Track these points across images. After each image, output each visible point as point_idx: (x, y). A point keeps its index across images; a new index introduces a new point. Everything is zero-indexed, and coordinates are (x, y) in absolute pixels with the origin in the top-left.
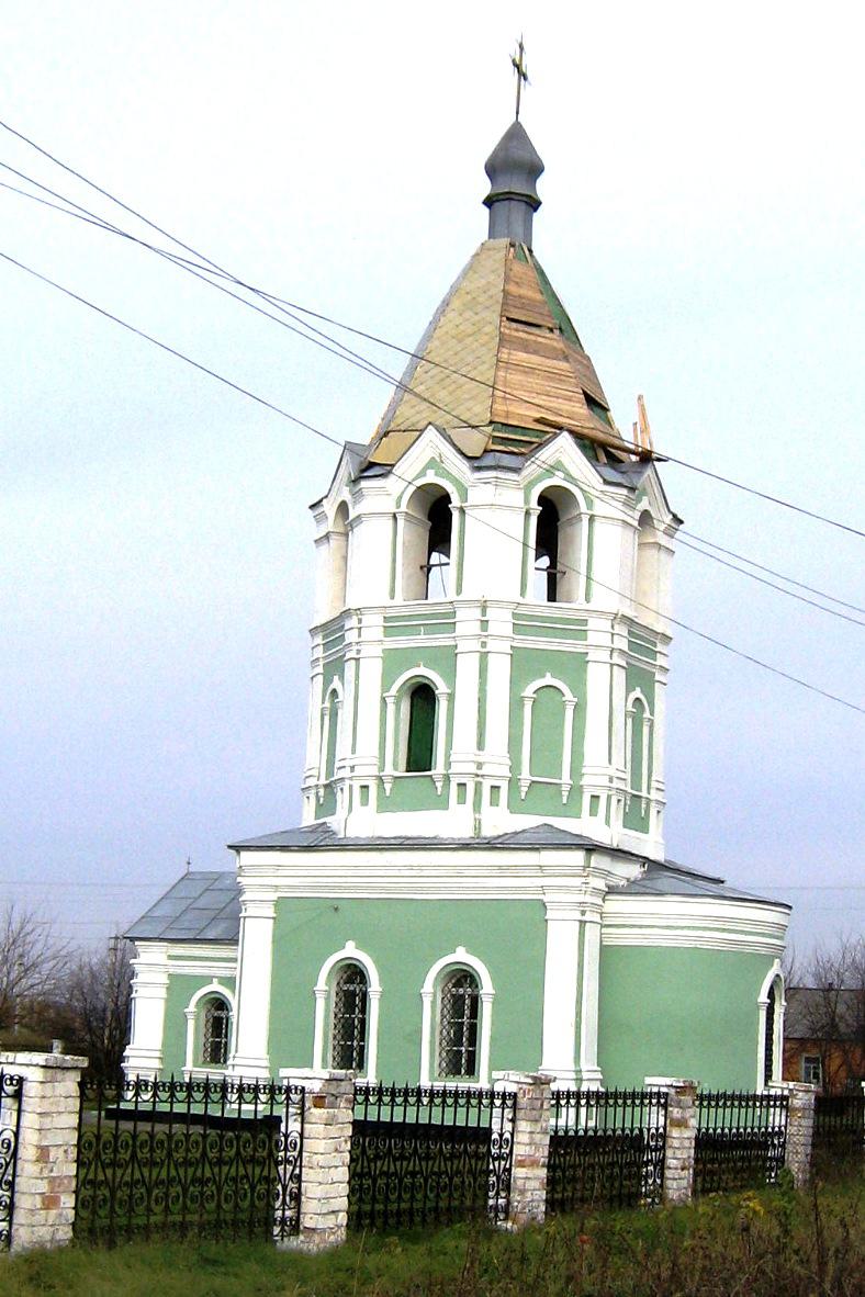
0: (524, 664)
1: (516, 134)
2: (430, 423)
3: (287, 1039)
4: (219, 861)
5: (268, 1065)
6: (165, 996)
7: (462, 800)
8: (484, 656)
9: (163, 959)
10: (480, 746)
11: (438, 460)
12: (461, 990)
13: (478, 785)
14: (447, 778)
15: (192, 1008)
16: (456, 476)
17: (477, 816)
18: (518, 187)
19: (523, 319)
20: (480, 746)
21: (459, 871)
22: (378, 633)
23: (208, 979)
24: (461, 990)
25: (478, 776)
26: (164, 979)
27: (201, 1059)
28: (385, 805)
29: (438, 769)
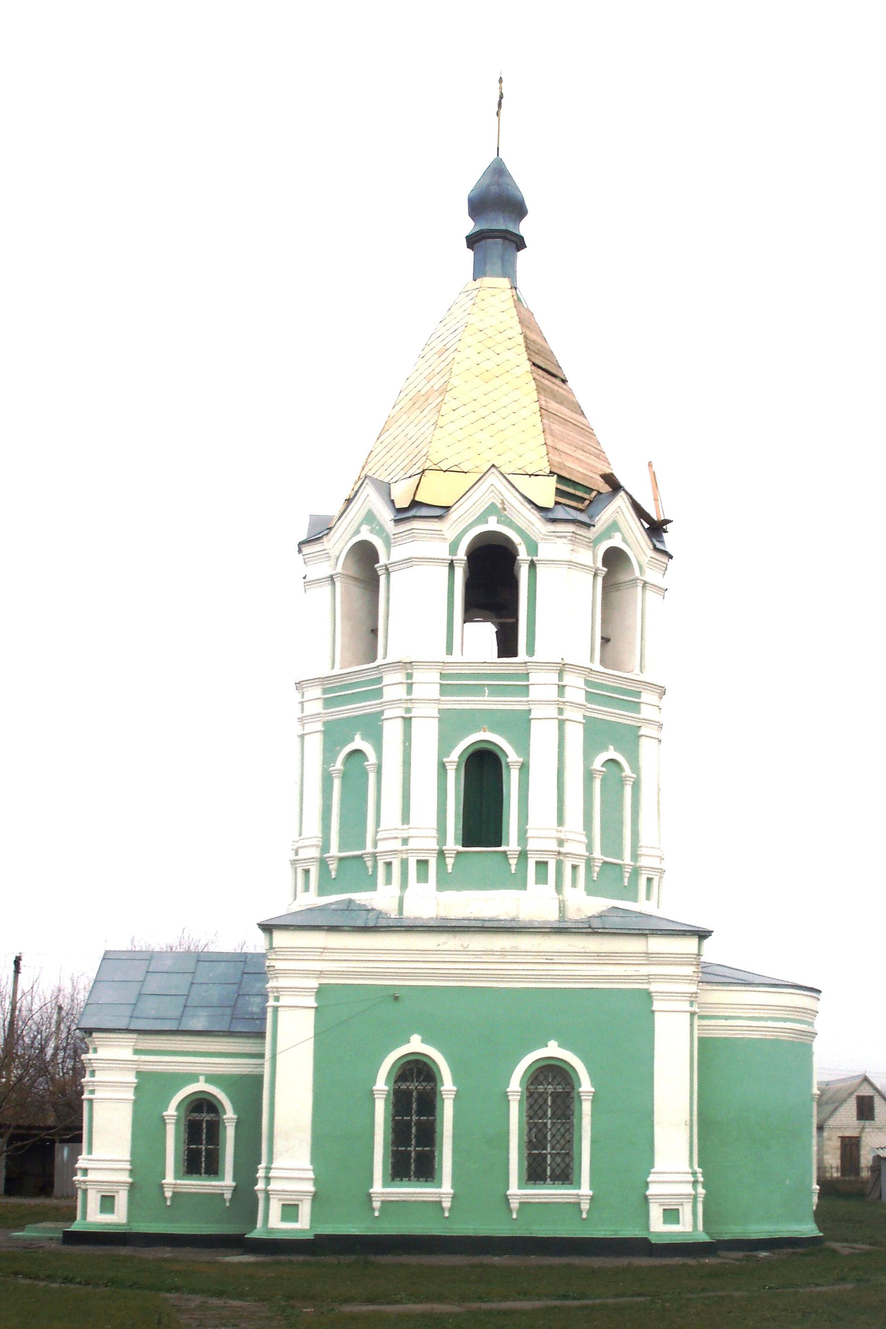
0: (597, 734)
1: (498, 170)
2: (493, 466)
3: (333, 1140)
4: (257, 943)
5: (129, 1167)
6: (133, 1097)
7: (542, 878)
8: (407, 721)
9: (126, 1053)
10: (561, 821)
11: (500, 506)
12: (552, 1090)
13: (404, 863)
14: (523, 855)
15: (171, 1111)
16: (524, 528)
17: (561, 897)
18: (500, 224)
19: (544, 367)
20: (561, 821)
21: (550, 958)
22: (434, 691)
23: (193, 1078)
24: (552, 1090)
25: (559, 853)
26: (132, 1078)
27: (183, 1169)
28: (445, 882)
29: (512, 845)
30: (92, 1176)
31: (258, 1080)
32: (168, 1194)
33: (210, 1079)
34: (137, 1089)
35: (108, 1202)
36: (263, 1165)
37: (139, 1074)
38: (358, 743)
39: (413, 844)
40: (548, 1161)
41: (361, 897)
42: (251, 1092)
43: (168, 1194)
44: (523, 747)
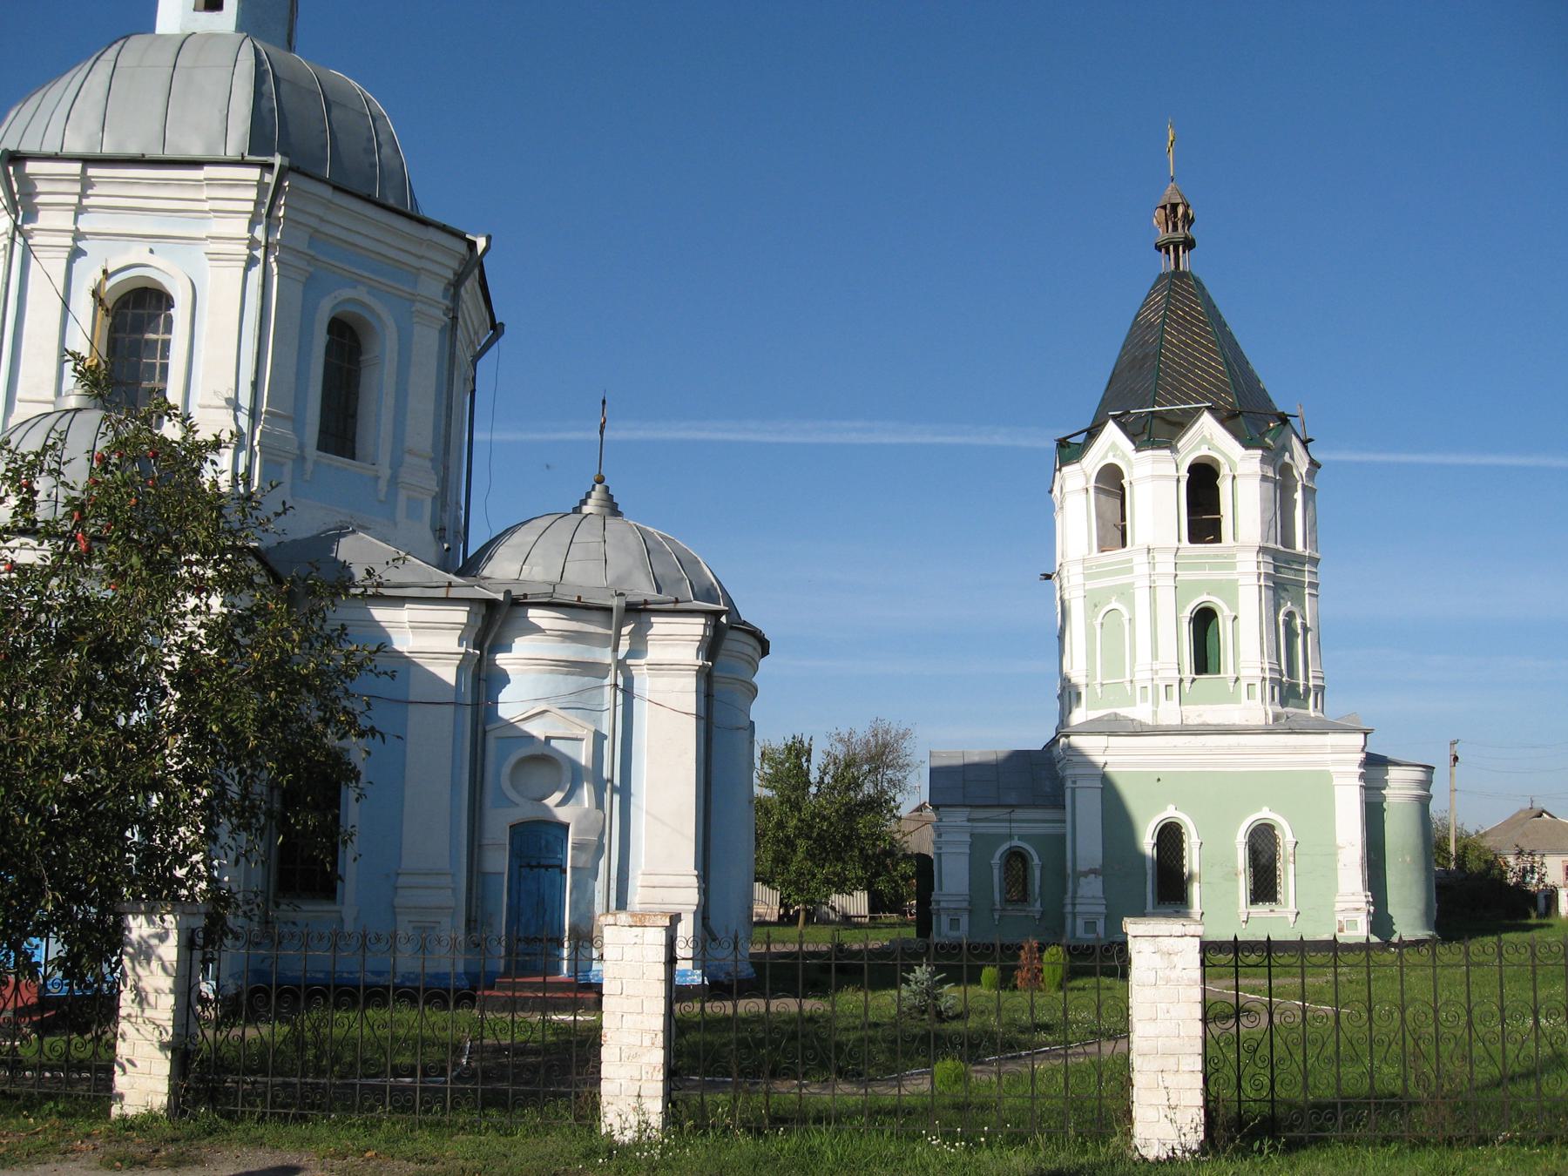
26: (967, 838)
30: (943, 904)
31: (1061, 839)
35: (954, 923)
36: (1069, 894)
37: (972, 835)
40: (1264, 886)
41: (1124, 711)
42: (1056, 846)
44: (1233, 604)
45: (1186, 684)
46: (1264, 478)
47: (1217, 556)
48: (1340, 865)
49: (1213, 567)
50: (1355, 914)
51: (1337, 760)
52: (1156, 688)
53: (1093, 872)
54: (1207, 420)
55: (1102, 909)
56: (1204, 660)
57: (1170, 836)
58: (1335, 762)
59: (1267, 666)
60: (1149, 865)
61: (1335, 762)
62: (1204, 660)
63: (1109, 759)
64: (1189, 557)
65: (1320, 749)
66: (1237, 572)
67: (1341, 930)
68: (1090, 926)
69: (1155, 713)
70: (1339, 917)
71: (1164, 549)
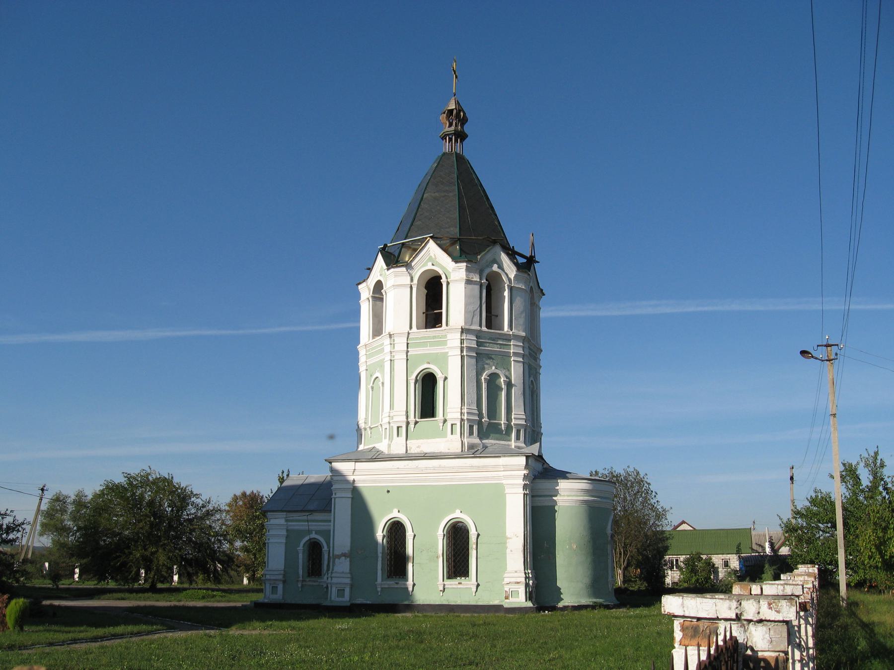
9: (282, 521)
23: (309, 532)
26: (285, 533)
32: (379, 589)
33: (317, 532)
34: (287, 537)
37: (287, 530)
38: (377, 374)
39: (395, 419)
43: (379, 589)
44: (444, 369)
45: (412, 426)
46: (468, 282)
47: (434, 337)
48: (508, 551)
49: (433, 344)
50: (517, 586)
51: (508, 473)
52: (391, 428)
53: (344, 555)
54: (432, 246)
55: (348, 581)
56: (427, 408)
57: (396, 530)
58: (506, 477)
59: (465, 411)
60: (380, 550)
61: (506, 477)
62: (427, 408)
63: (356, 478)
64: (417, 339)
65: (495, 469)
66: (447, 351)
67: (507, 598)
68: (341, 592)
69: (389, 446)
70: (507, 588)
71: (400, 334)
